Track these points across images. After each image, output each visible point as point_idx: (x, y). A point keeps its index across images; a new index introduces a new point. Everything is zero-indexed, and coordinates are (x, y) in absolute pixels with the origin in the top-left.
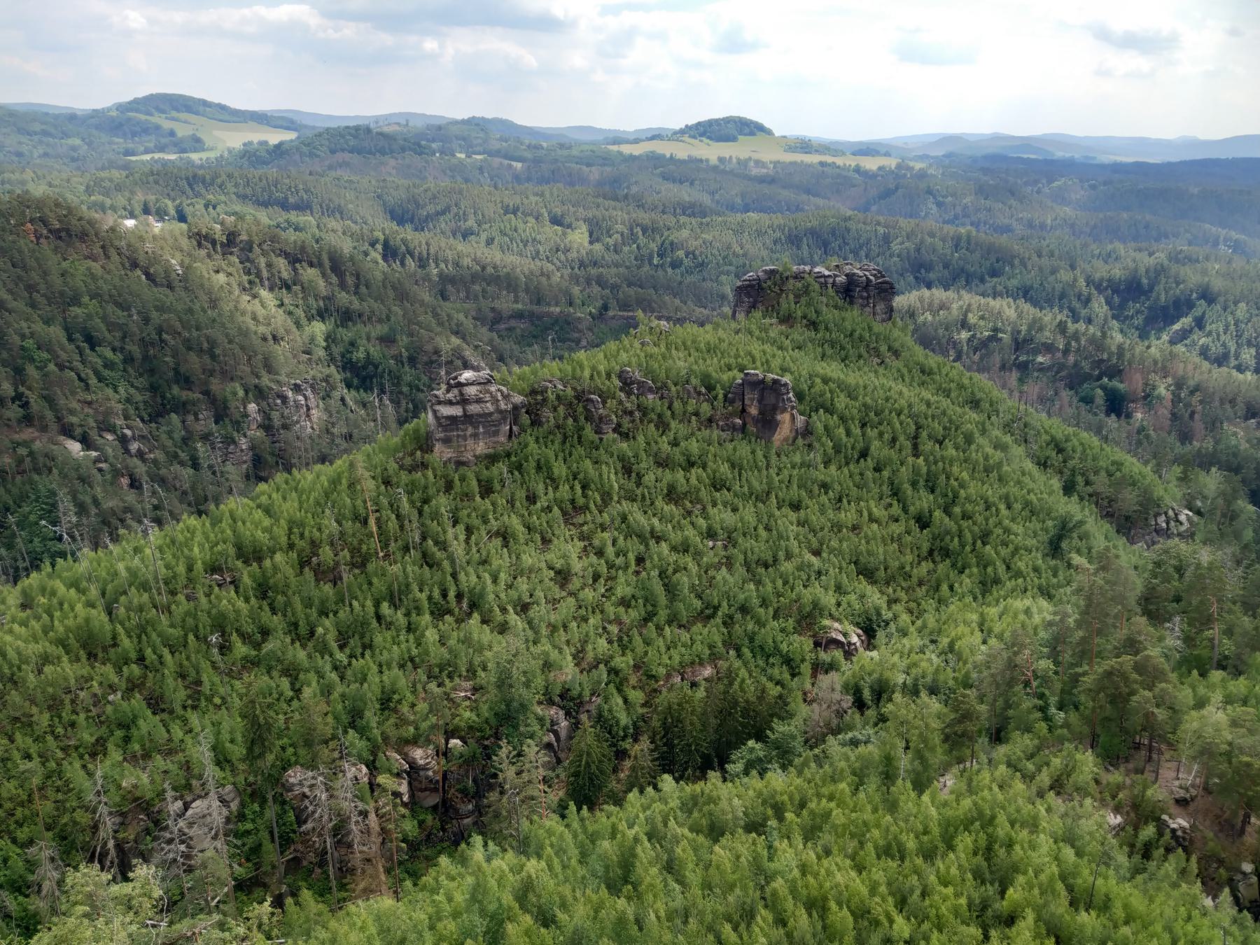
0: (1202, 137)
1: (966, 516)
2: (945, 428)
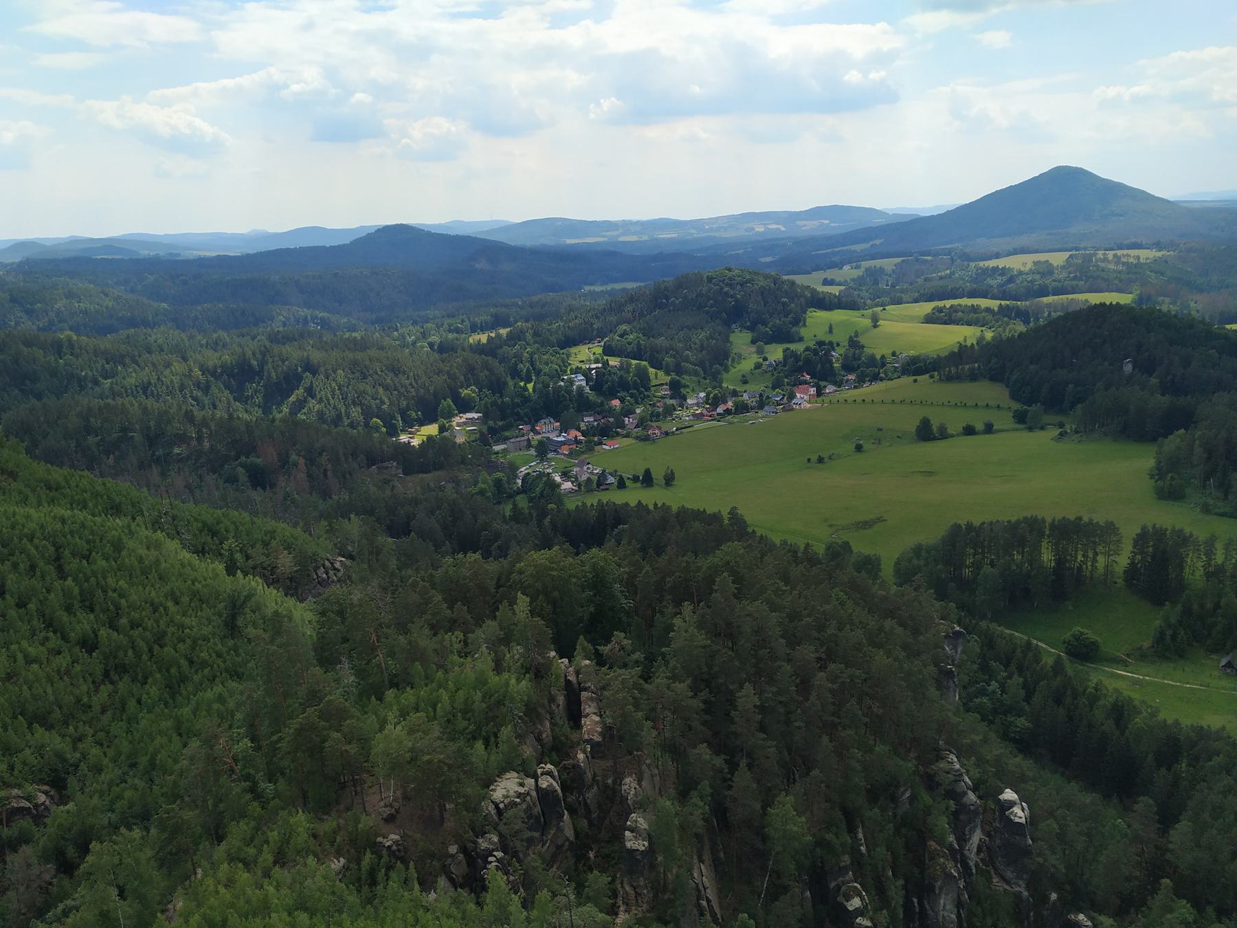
0: (271, 231)
1: (134, 625)
2: (88, 542)
